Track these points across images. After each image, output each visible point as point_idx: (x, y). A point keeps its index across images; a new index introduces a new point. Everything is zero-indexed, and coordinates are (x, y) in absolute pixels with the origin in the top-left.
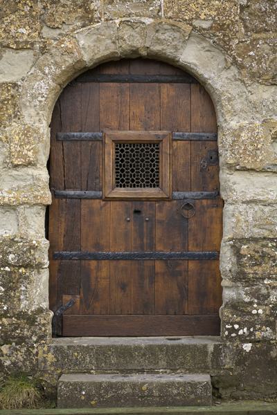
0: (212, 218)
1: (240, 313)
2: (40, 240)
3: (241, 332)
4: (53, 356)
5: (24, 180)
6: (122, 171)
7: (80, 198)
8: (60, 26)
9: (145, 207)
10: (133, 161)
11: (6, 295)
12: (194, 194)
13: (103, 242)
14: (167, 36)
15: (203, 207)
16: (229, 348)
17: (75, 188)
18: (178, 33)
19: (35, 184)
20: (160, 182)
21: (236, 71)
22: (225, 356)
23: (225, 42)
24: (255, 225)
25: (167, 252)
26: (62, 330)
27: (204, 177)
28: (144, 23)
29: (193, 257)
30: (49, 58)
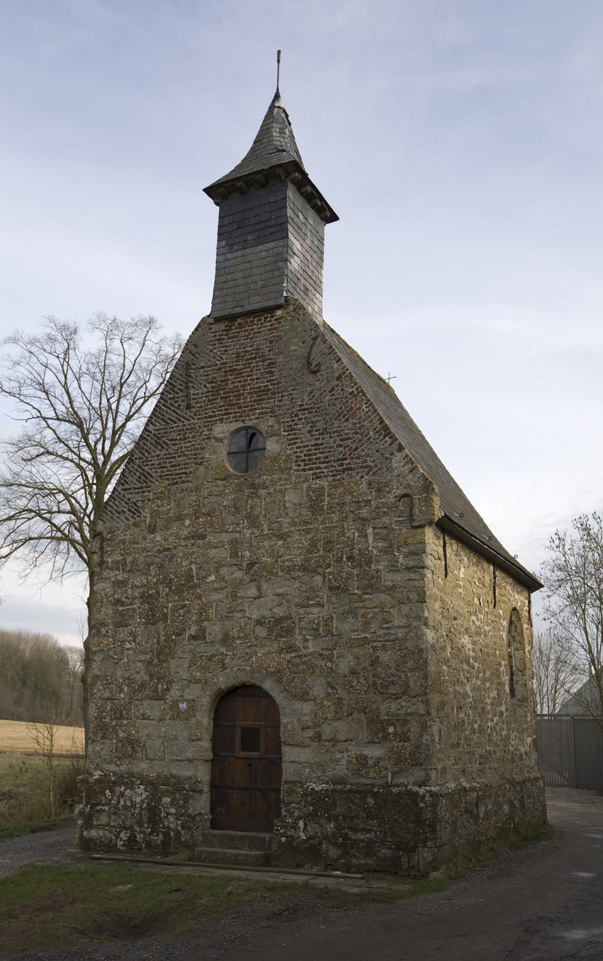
5: (197, 747)
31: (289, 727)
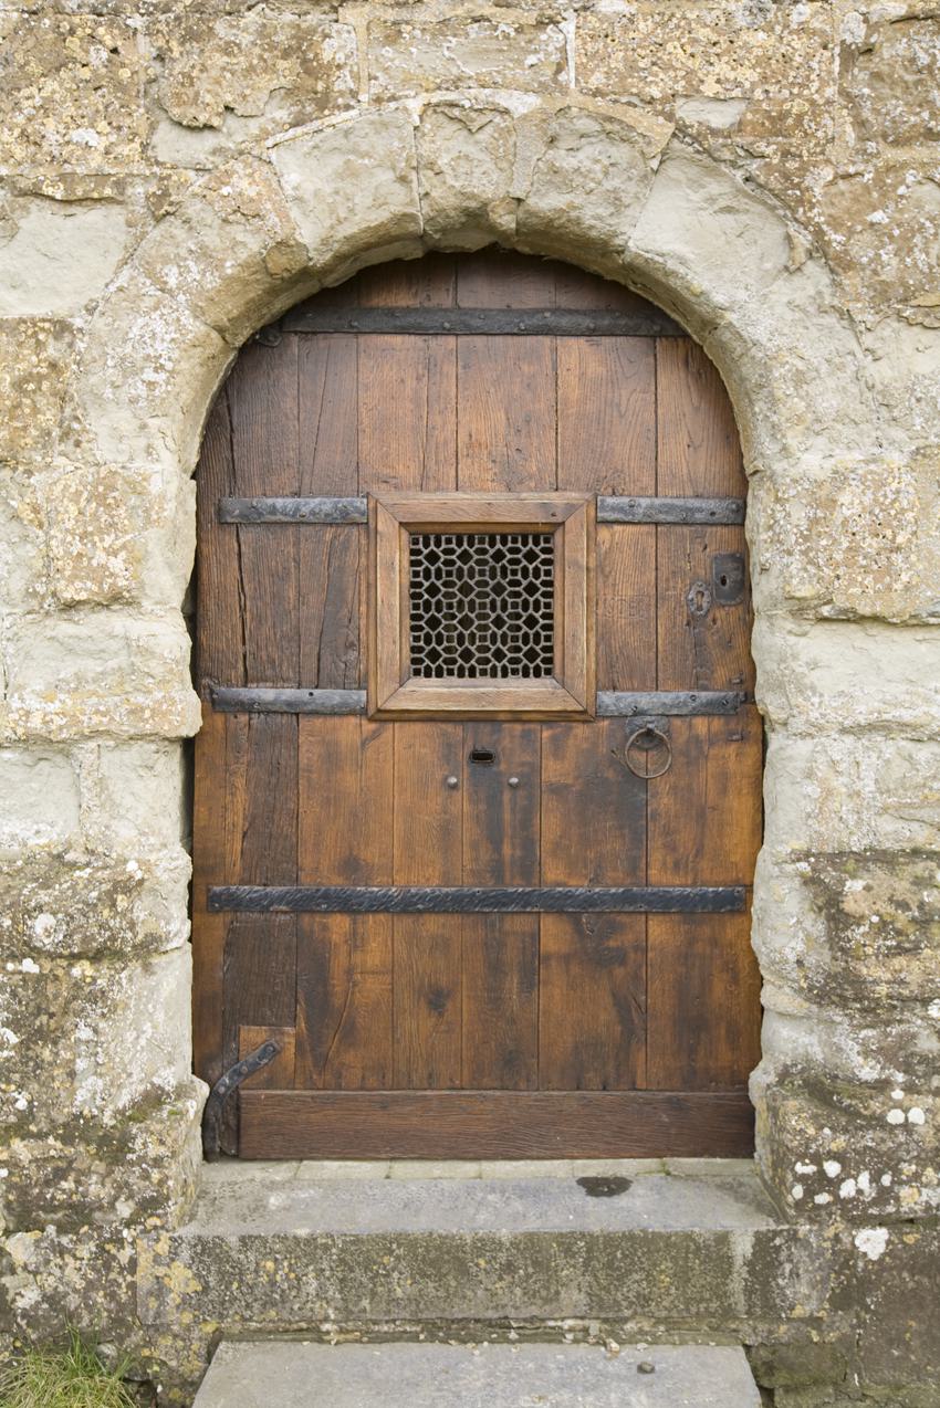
0: (724, 779)
1: (843, 1120)
2: (153, 858)
3: (847, 1189)
4: (189, 1274)
6: (433, 623)
7: (295, 712)
8: (216, 122)
9: (506, 742)
10: (466, 590)
11: (25, 1060)
12: (667, 697)
13: (370, 854)
14: (588, 157)
15: (697, 740)
16: (806, 1244)
17: (278, 681)
18: (625, 148)
19: (133, 669)
20: (557, 660)
21: (825, 279)
22: (795, 1274)
23: (786, 176)
24: (885, 809)
25: (579, 887)
26: (239, 1143)
27: (699, 644)
28: (506, 112)
29: (664, 904)
30: (180, 232)
31: (850, 501)
